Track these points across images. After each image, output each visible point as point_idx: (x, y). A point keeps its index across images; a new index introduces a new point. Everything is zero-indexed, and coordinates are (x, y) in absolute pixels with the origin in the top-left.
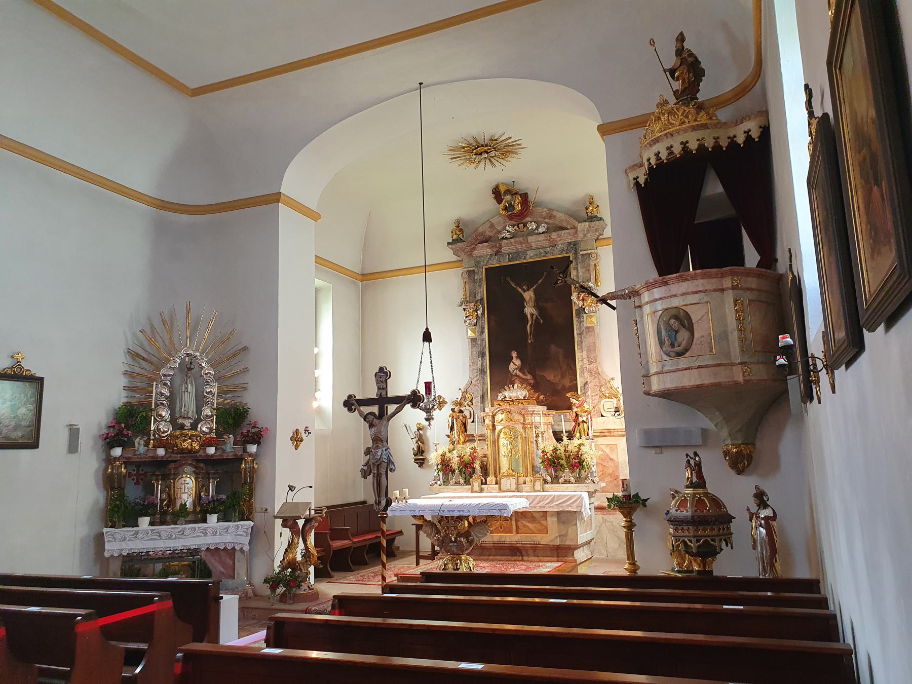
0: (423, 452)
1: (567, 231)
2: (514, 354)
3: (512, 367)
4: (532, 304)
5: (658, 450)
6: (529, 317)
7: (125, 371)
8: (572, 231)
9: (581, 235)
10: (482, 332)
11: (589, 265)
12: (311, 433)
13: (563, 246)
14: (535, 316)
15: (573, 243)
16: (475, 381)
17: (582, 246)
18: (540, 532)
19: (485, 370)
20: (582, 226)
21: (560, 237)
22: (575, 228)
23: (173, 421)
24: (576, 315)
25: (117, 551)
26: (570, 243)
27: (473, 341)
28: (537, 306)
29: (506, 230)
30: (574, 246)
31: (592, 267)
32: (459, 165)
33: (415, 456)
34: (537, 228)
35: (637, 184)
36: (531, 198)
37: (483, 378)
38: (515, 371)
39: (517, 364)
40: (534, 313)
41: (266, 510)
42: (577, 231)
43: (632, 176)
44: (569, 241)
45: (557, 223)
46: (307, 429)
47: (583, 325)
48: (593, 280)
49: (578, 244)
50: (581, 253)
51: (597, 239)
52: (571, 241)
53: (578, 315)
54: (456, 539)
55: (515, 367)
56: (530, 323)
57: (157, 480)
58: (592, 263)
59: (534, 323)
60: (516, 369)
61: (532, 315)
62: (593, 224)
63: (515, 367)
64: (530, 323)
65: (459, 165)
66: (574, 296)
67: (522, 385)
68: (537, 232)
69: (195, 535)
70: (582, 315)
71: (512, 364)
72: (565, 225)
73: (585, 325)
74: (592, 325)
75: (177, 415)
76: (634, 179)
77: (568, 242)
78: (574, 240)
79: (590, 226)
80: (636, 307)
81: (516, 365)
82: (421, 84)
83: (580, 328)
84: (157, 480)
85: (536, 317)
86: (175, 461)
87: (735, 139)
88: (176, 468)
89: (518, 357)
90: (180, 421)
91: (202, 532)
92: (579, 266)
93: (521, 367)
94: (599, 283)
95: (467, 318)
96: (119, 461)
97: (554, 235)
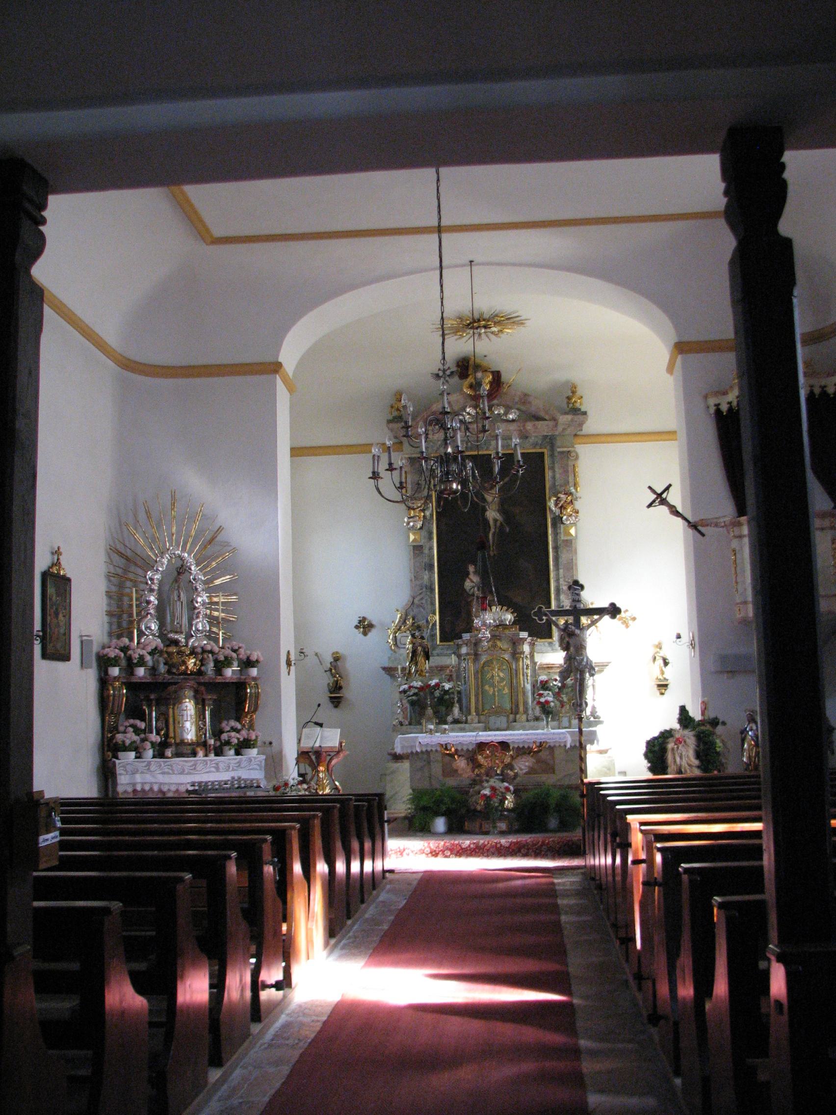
0: (341, 688)
1: (546, 422)
2: (471, 569)
3: (468, 584)
4: (495, 506)
5: (730, 675)
6: (491, 523)
7: (109, 573)
8: (551, 423)
9: (560, 429)
10: (430, 538)
11: (567, 465)
12: (307, 656)
13: (537, 440)
14: (498, 524)
15: (549, 437)
16: (419, 601)
17: (558, 443)
18: (545, 771)
19: (433, 587)
20: (564, 419)
21: (537, 428)
22: (554, 419)
23: (162, 635)
24: (552, 524)
25: (174, 785)
26: (545, 437)
27: (417, 549)
28: (502, 510)
29: (466, 412)
30: (550, 441)
31: (570, 469)
32: (456, 340)
33: (331, 693)
34: (506, 414)
35: (718, 412)
36: (504, 378)
37: (431, 598)
38: (472, 590)
39: (475, 581)
40: (498, 518)
41: (271, 743)
42: (557, 424)
43: (712, 401)
44: (545, 434)
45: (533, 409)
46: (304, 651)
47: (560, 537)
48: (571, 484)
49: (555, 438)
50: (559, 450)
51: (576, 435)
52: (547, 434)
53: (554, 525)
54: (502, 771)
55: (472, 584)
56: (492, 530)
57: (150, 707)
58: (571, 463)
59: (497, 531)
60: (473, 587)
61: (495, 521)
62: (576, 418)
63: (472, 584)
64: (492, 530)
65: (456, 340)
66: (552, 501)
67: (502, 607)
68: (505, 418)
69: (208, 770)
70: (558, 525)
71: (468, 580)
72: (542, 414)
73: (562, 538)
74: (569, 538)
75: (169, 628)
76: (716, 405)
77: (543, 436)
78: (550, 434)
79: (572, 420)
80: (735, 537)
81: (473, 582)
82: (471, 262)
83: (555, 540)
84: (150, 707)
85: (501, 523)
86: (175, 684)
87: (825, 389)
88: (176, 692)
89: (475, 573)
90: (171, 635)
91: (258, 765)
92: (556, 465)
93: (483, 583)
94: (578, 489)
95: (411, 520)
96: (118, 681)
97: (529, 426)
